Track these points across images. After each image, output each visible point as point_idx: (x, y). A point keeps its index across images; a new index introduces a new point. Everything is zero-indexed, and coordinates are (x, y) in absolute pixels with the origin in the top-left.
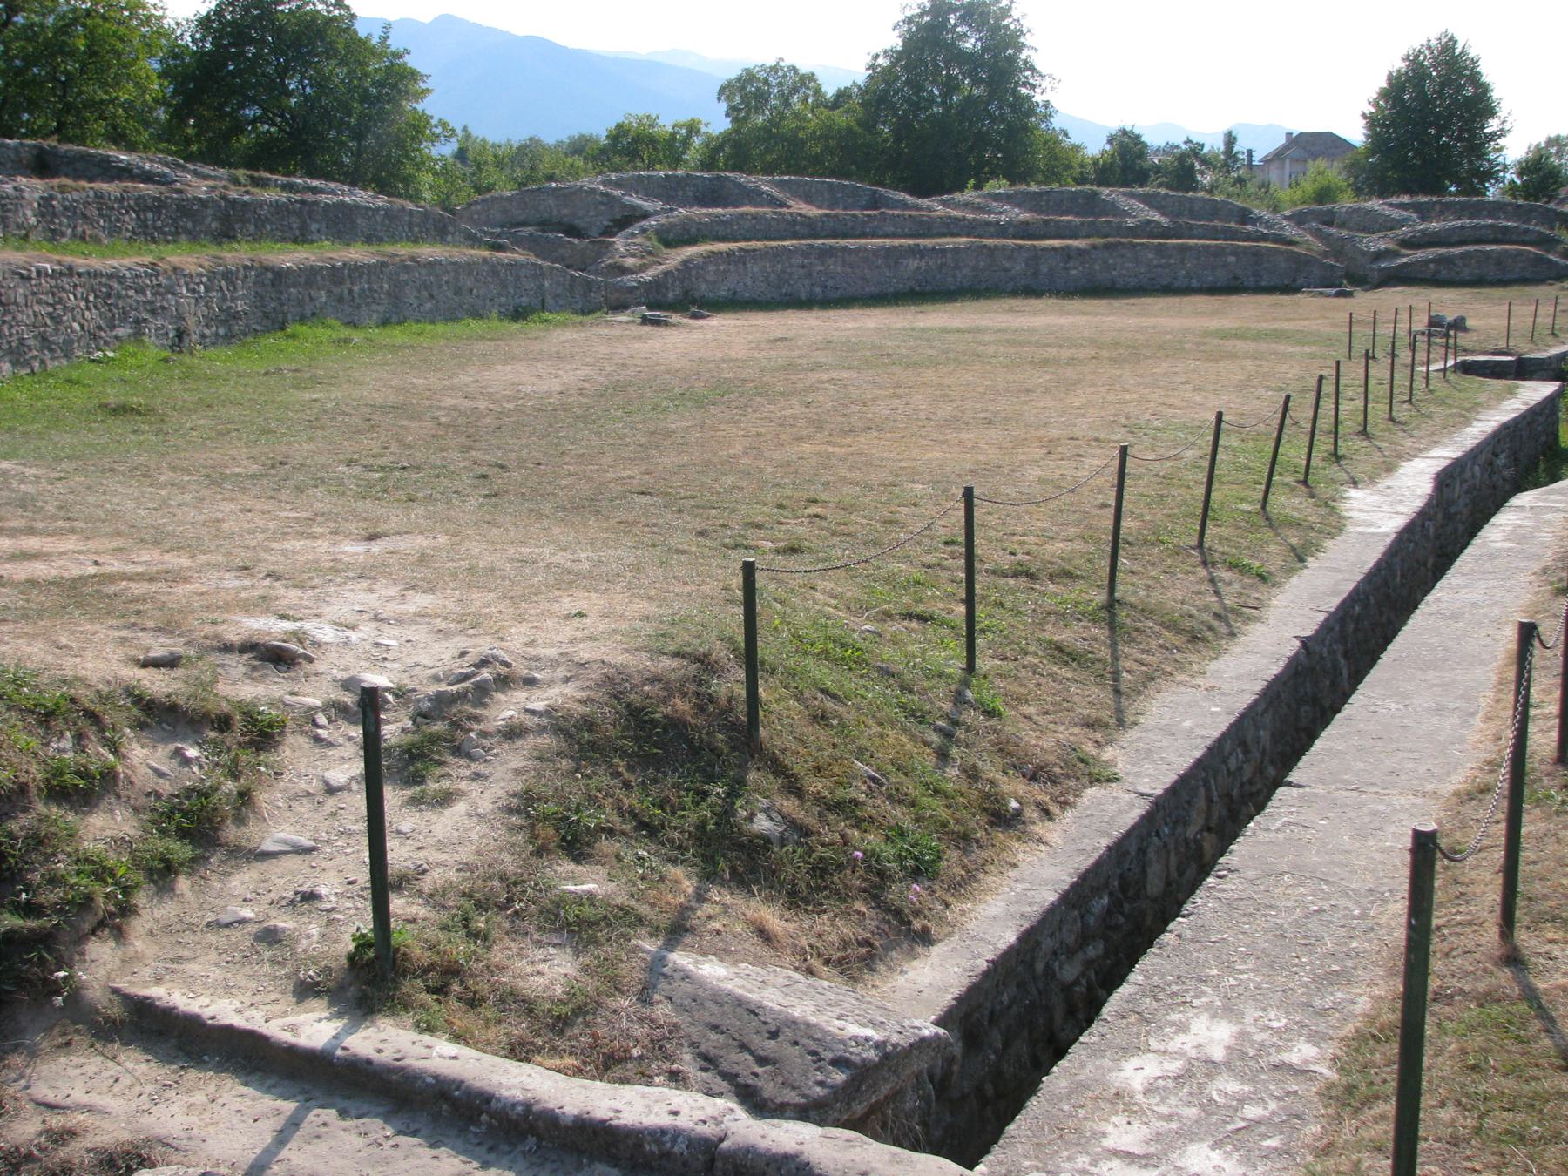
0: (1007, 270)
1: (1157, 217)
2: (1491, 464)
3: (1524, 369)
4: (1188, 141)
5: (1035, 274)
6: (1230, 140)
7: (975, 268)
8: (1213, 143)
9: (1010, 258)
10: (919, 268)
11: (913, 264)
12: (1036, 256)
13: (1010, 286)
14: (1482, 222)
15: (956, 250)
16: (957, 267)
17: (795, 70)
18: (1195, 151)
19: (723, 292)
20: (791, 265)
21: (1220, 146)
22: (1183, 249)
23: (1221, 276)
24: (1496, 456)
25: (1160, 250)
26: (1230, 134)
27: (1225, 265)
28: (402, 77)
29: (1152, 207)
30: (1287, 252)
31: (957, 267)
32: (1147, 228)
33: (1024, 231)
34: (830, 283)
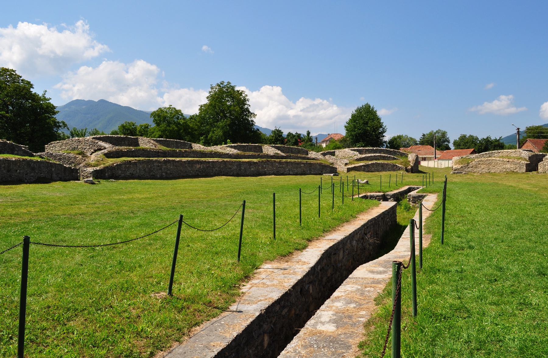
0: (230, 168)
1: (279, 152)
2: (363, 238)
3: (385, 198)
4: (297, 133)
5: (240, 170)
6: (309, 133)
7: (219, 168)
8: (304, 133)
9: (230, 165)
10: (200, 167)
11: (198, 166)
12: (240, 163)
13: (232, 173)
14: (377, 154)
15: (213, 162)
16: (213, 167)
17: (175, 109)
18: (299, 136)
19: (128, 173)
20: (154, 166)
21: (306, 134)
22: (286, 162)
23: (299, 170)
24: (366, 234)
25: (280, 163)
26: (308, 131)
27: (301, 167)
28: (52, 108)
29: (279, 150)
30: (307, 163)
31: (213, 167)
32: (276, 156)
33: (237, 156)
34: (168, 172)
